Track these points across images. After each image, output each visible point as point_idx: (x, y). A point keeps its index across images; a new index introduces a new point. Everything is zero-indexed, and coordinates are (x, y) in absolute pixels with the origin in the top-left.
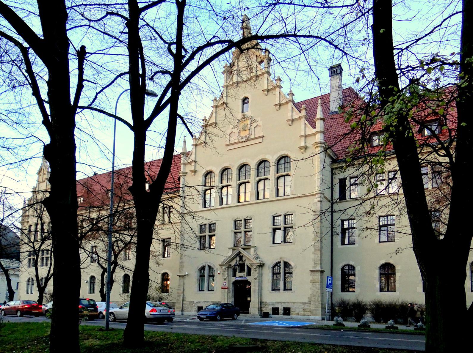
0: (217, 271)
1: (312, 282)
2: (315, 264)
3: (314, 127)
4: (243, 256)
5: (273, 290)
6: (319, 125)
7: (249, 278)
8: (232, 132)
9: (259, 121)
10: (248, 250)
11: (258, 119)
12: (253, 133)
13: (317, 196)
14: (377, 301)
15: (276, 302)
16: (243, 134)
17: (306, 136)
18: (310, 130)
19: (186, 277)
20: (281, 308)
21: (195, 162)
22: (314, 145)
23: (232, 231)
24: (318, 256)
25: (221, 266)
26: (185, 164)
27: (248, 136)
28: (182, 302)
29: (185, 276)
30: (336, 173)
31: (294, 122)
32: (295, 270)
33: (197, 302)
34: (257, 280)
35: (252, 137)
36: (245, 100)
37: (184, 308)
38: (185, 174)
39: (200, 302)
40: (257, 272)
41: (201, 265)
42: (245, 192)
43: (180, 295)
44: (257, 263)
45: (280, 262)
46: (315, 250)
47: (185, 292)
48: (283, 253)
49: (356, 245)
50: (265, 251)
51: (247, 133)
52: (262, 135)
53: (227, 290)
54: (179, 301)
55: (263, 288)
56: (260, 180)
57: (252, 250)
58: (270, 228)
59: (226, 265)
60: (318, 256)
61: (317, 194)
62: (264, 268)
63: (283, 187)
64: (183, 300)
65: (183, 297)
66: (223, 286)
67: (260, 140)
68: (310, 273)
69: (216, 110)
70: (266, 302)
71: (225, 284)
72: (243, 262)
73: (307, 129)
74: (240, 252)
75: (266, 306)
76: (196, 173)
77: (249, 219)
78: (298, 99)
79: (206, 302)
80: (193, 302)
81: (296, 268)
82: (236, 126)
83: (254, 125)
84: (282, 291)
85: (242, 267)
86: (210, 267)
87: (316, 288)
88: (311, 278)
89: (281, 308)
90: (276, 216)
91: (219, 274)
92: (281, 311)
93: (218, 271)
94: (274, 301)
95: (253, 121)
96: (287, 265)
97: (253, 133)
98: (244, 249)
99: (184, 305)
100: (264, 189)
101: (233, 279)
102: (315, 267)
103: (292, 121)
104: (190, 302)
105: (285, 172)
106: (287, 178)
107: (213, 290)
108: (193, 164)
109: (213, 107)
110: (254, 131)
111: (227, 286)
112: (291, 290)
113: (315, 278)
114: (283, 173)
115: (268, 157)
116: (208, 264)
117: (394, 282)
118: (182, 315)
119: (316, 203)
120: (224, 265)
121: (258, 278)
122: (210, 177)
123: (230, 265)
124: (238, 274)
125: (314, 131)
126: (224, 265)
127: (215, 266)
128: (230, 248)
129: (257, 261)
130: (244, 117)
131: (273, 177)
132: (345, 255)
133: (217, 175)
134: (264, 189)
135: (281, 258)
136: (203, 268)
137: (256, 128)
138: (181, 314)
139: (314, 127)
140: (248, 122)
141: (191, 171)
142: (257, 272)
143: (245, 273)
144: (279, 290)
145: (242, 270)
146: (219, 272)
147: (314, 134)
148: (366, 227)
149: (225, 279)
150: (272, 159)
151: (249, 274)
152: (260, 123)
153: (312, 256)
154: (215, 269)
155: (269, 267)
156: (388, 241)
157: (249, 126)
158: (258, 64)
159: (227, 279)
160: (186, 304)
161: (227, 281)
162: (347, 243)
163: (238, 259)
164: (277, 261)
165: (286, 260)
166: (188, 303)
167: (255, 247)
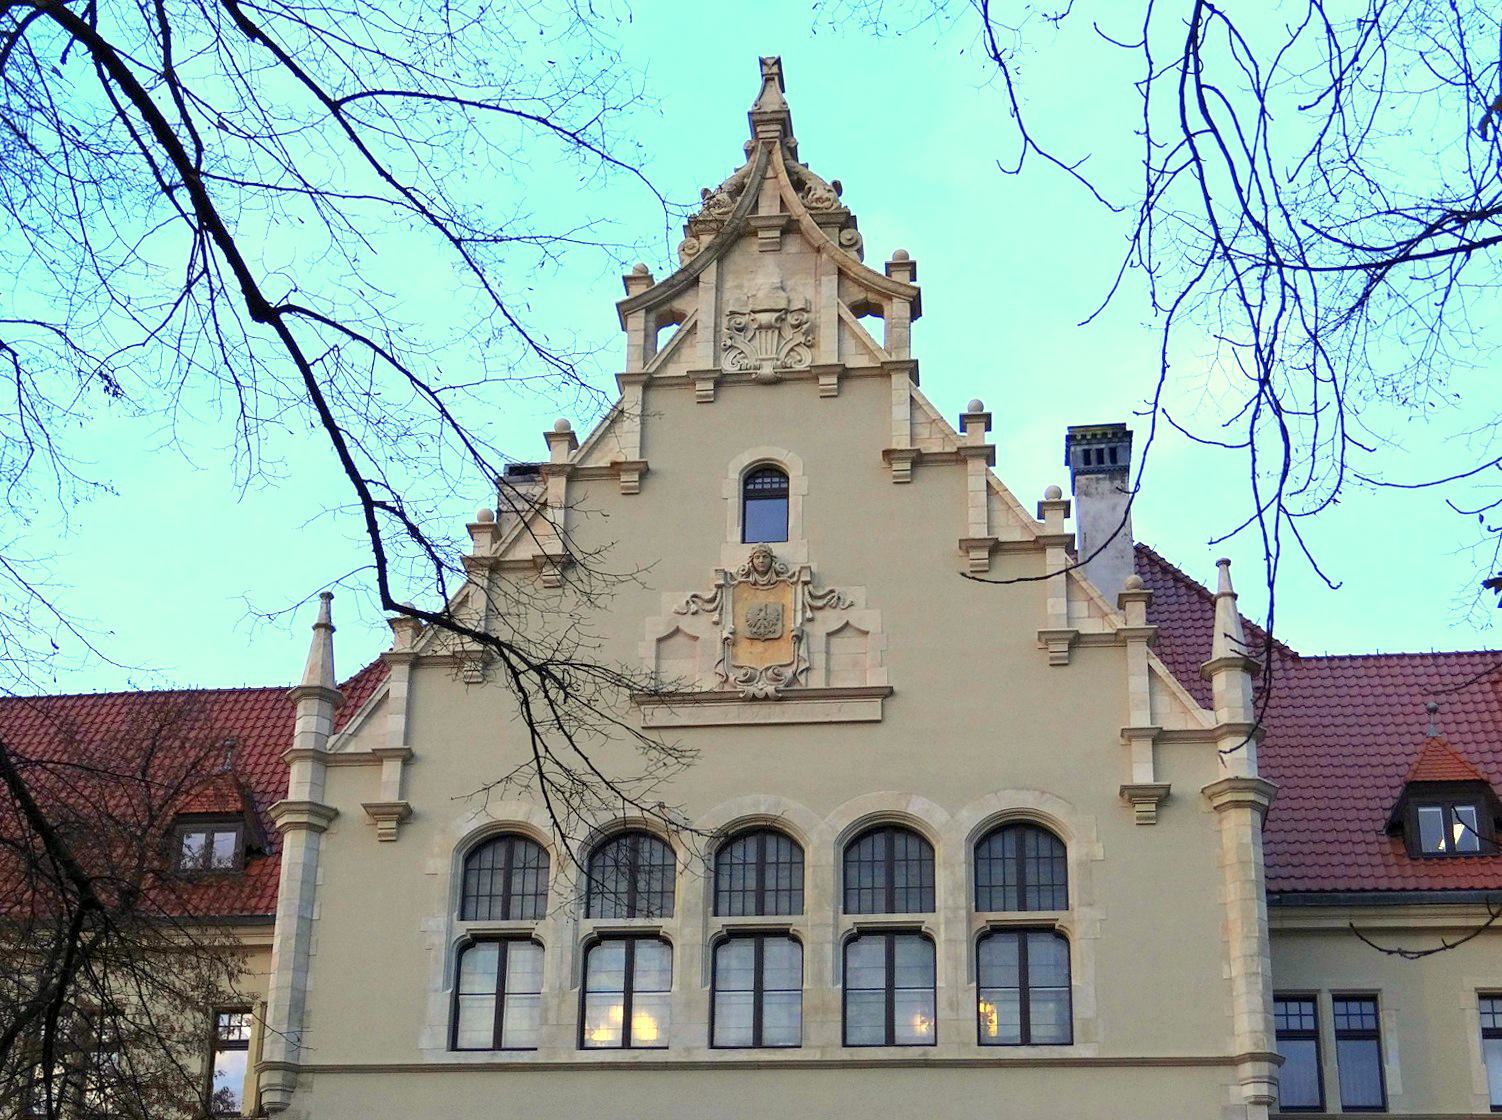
3: (1206, 701)
17: (1160, 738)
18: (1179, 712)
125: (1206, 720)
139: (1206, 701)
147: (1210, 737)
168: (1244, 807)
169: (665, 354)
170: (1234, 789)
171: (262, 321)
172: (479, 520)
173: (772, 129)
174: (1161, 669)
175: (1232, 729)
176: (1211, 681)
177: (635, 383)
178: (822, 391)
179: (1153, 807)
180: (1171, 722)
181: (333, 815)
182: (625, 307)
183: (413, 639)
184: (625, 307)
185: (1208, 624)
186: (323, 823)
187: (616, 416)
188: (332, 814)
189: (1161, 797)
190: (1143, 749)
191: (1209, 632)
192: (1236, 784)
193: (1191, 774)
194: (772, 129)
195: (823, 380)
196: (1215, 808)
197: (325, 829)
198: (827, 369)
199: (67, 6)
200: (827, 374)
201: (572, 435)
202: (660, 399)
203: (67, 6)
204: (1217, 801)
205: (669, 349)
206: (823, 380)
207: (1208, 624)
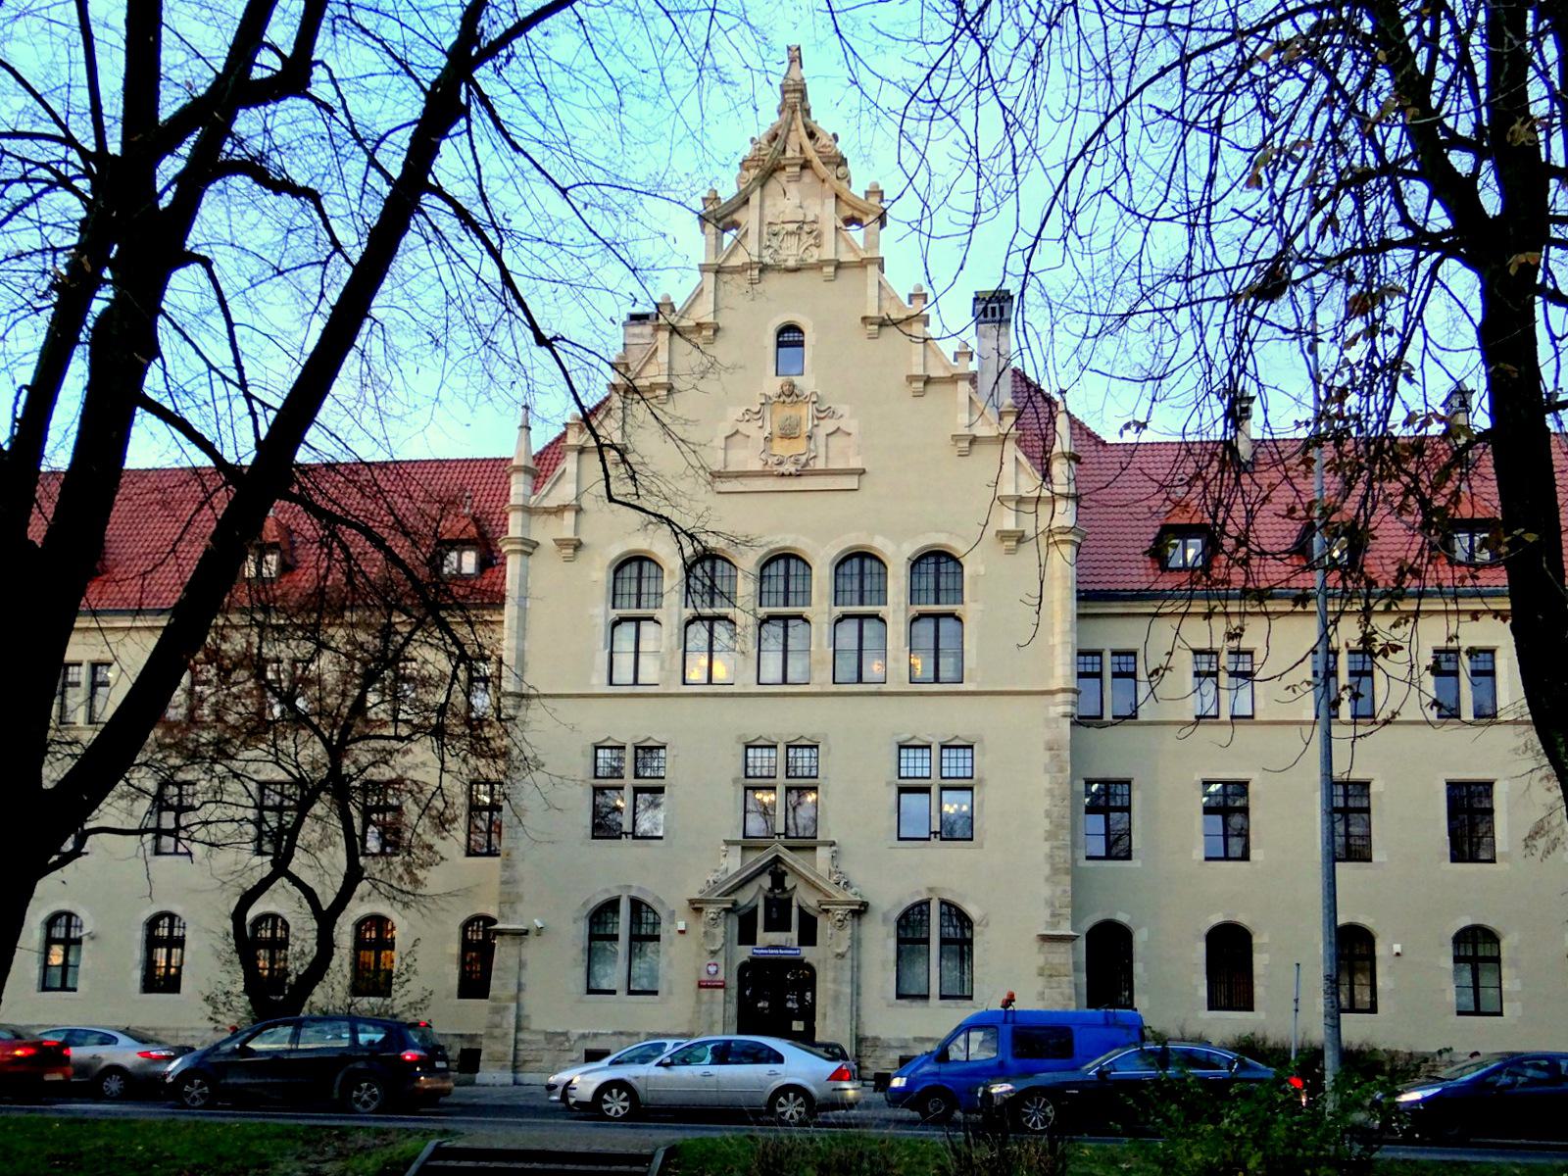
0: (673, 922)
1: (1047, 972)
2: (1053, 915)
4: (785, 874)
5: (899, 996)
6: (1060, 469)
7: (807, 953)
8: (737, 432)
9: (847, 415)
10: (807, 855)
11: (843, 409)
12: (822, 450)
13: (1060, 697)
14: (1259, 1034)
15: (916, 1039)
16: (781, 448)
19: (531, 939)
21: (579, 510)
23: (735, 781)
24: (1065, 891)
25: (696, 907)
26: (528, 510)
27: (803, 459)
28: (512, 1037)
29: (526, 932)
31: (975, 448)
32: (981, 933)
33: (584, 1036)
34: (847, 962)
35: (820, 464)
36: (789, 337)
37: (523, 1055)
38: (530, 550)
39: (595, 1035)
40: (848, 931)
41: (601, 898)
42: (637, 652)
43: (506, 1008)
44: (849, 903)
45: (927, 903)
46: (1055, 870)
47: (527, 999)
48: (941, 873)
49: (1135, 863)
50: (870, 859)
51: (799, 446)
52: (855, 463)
53: (721, 992)
54: (497, 1032)
55: (863, 989)
56: (621, 620)
57: (823, 853)
58: (888, 784)
59: (721, 902)
60: (1065, 891)
61: (1064, 690)
62: (865, 919)
63: (632, 656)
64: (518, 1028)
65: (518, 1017)
66: (705, 977)
67: (851, 482)
68: (1035, 946)
70: (876, 1039)
71: (712, 969)
72: (786, 896)
74: (777, 860)
75: (878, 1053)
76: (580, 553)
77: (658, 748)
79: (621, 1033)
80: (565, 1034)
81: (987, 924)
82: (751, 415)
83: (828, 425)
84: (934, 1000)
85: (778, 913)
86: (637, 905)
87: (1062, 994)
88: (1040, 960)
90: (796, 747)
91: (682, 932)
93: (676, 923)
94: (909, 1036)
95: (823, 413)
96: (957, 917)
97: (822, 450)
98: (791, 848)
99: (521, 1046)
100: (860, 649)
101: (745, 953)
102: (1055, 925)
104: (550, 1036)
105: (639, 606)
106: (647, 628)
107: (655, 993)
108: (569, 517)
110: (827, 446)
111: (721, 976)
112: (970, 998)
113: (1056, 961)
114: (933, 608)
115: (879, 544)
116: (634, 893)
118: (516, 1083)
119: (1055, 720)
120: (714, 902)
121: (849, 955)
122: (635, 574)
123: (735, 903)
124: (764, 938)
126: (714, 902)
127: (662, 903)
128: (728, 843)
129: (849, 895)
130: (790, 393)
131: (826, 618)
132: (1120, 894)
133: (672, 572)
134: (860, 649)
135: (931, 890)
136: (612, 906)
137: (831, 438)
138: (511, 1081)
140: (806, 412)
141: (561, 543)
142: (848, 931)
143: (794, 934)
144: (926, 997)
145: (777, 923)
146: (681, 926)
149: (714, 953)
150: (897, 557)
151: (808, 936)
152: (849, 424)
153: (1045, 891)
154: (663, 915)
155: (885, 920)
156: (1108, 857)
157: (807, 427)
158: (840, 224)
159: (722, 953)
160: (530, 1042)
161: (721, 961)
163: (766, 881)
164: (918, 899)
165: (947, 897)
166: (541, 1037)
167: (833, 844)
174: (1023, 458)
201: (672, 304)
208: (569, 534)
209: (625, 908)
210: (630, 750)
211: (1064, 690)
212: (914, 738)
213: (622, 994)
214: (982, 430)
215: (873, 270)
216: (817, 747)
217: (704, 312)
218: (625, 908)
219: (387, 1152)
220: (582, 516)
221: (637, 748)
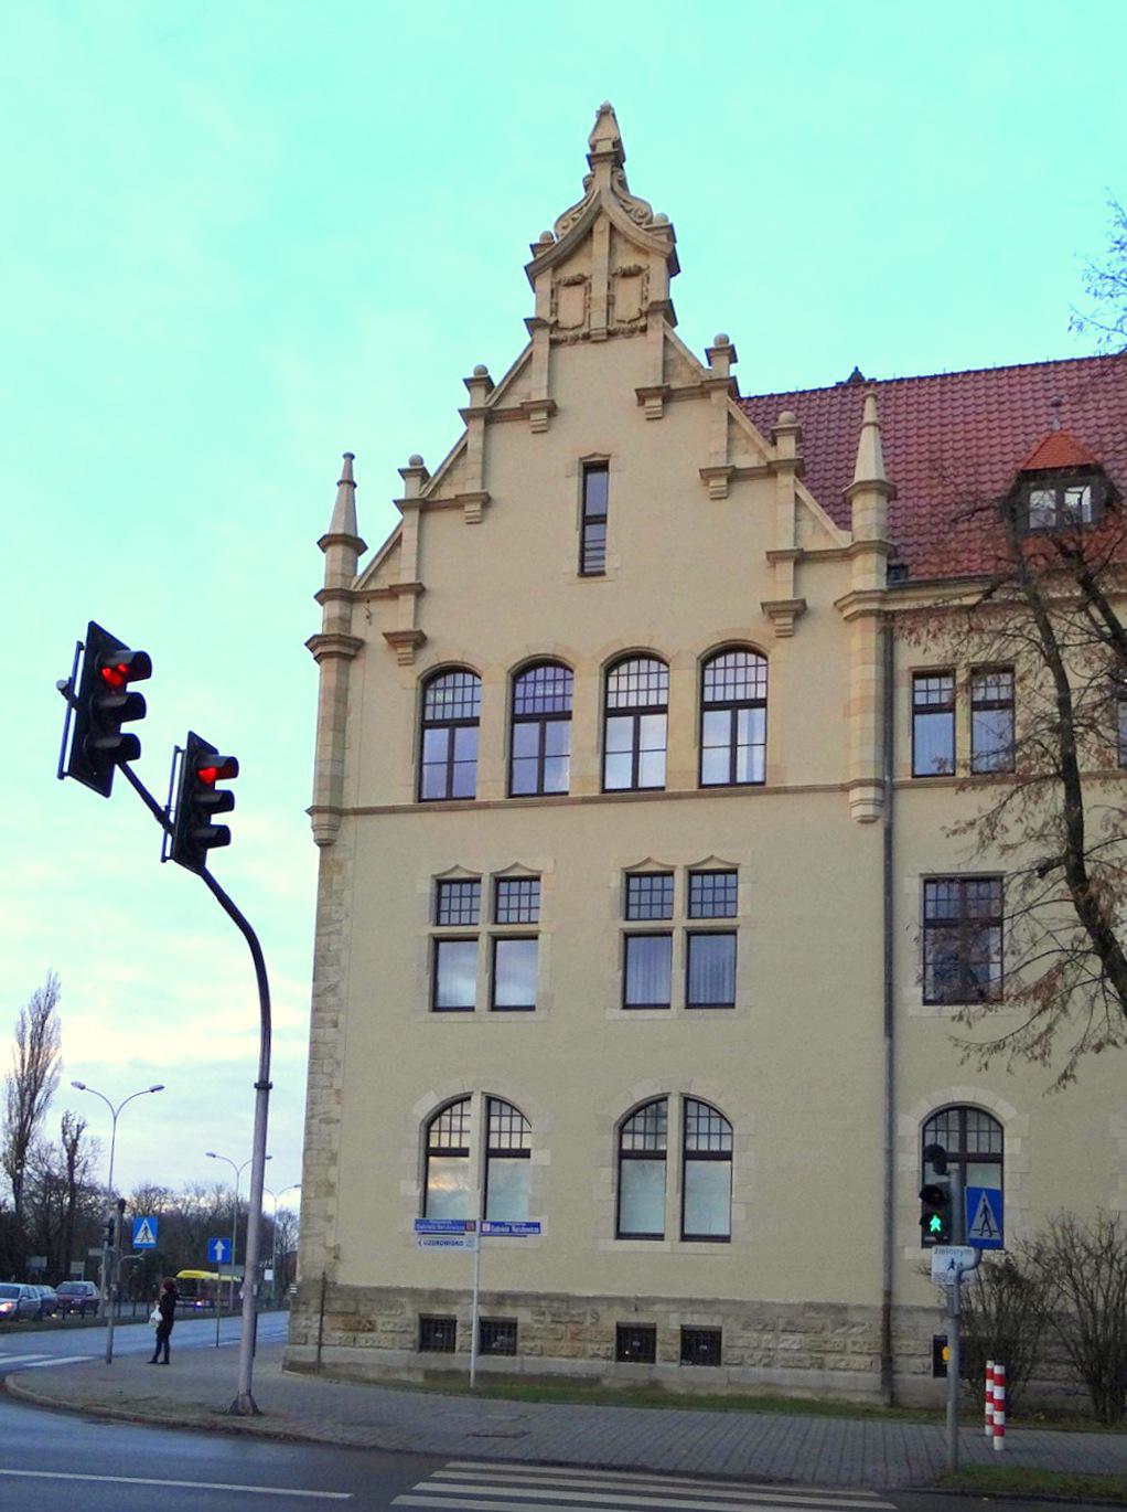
3: (844, 523)
17: (801, 558)
18: (823, 534)
20: (669, 1327)
21: (419, 591)
22: (840, 605)
30: (1116, 812)
61: (862, 783)
69: (486, 434)
73: (806, 525)
78: (752, 383)
89: (669, 1327)
92: (668, 1344)
103: (730, 481)
108: (407, 602)
109: (467, 415)
117: (1029, 1429)
125: (842, 539)
136: (652, 1107)
139: (844, 523)
141: (395, 639)
147: (846, 555)
148: (956, 1045)
162: (447, 922)
168: (332, 657)
169: (503, 388)
170: (859, 601)
171: (361, 540)
172: (475, 373)
173: (608, 157)
174: (805, 494)
175: (863, 547)
176: (851, 504)
177: (478, 417)
178: (534, 426)
179: (790, 620)
180: (813, 544)
181: (359, 644)
182: (534, 268)
183: (421, 485)
184: (534, 268)
185: (852, 456)
186: (352, 652)
187: (461, 450)
188: (358, 644)
189: (799, 611)
190: (787, 568)
191: (851, 464)
192: (859, 596)
193: (824, 587)
194: (608, 157)
195: (467, 508)
196: (846, 618)
197: (353, 657)
198: (471, 498)
199: (393, 1503)
200: (471, 501)
201: (489, 379)
202: (436, 521)
203: (393, 1503)
204: (846, 613)
205: (506, 383)
206: (533, 417)
207: (852, 456)
208: (405, 625)
209: (674, 1108)
210: (486, 883)
211: (862, 783)
212: (648, 860)
213: (672, 1243)
214: (744, 461)
215: (657, 325)
216: (735, 872)
217: (534, 388)
218: (674, 1108)
219: (1044, 1398)
220: (427, 602)
221: (692, 873)
